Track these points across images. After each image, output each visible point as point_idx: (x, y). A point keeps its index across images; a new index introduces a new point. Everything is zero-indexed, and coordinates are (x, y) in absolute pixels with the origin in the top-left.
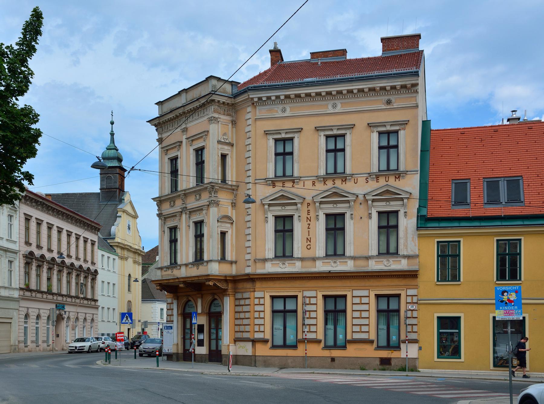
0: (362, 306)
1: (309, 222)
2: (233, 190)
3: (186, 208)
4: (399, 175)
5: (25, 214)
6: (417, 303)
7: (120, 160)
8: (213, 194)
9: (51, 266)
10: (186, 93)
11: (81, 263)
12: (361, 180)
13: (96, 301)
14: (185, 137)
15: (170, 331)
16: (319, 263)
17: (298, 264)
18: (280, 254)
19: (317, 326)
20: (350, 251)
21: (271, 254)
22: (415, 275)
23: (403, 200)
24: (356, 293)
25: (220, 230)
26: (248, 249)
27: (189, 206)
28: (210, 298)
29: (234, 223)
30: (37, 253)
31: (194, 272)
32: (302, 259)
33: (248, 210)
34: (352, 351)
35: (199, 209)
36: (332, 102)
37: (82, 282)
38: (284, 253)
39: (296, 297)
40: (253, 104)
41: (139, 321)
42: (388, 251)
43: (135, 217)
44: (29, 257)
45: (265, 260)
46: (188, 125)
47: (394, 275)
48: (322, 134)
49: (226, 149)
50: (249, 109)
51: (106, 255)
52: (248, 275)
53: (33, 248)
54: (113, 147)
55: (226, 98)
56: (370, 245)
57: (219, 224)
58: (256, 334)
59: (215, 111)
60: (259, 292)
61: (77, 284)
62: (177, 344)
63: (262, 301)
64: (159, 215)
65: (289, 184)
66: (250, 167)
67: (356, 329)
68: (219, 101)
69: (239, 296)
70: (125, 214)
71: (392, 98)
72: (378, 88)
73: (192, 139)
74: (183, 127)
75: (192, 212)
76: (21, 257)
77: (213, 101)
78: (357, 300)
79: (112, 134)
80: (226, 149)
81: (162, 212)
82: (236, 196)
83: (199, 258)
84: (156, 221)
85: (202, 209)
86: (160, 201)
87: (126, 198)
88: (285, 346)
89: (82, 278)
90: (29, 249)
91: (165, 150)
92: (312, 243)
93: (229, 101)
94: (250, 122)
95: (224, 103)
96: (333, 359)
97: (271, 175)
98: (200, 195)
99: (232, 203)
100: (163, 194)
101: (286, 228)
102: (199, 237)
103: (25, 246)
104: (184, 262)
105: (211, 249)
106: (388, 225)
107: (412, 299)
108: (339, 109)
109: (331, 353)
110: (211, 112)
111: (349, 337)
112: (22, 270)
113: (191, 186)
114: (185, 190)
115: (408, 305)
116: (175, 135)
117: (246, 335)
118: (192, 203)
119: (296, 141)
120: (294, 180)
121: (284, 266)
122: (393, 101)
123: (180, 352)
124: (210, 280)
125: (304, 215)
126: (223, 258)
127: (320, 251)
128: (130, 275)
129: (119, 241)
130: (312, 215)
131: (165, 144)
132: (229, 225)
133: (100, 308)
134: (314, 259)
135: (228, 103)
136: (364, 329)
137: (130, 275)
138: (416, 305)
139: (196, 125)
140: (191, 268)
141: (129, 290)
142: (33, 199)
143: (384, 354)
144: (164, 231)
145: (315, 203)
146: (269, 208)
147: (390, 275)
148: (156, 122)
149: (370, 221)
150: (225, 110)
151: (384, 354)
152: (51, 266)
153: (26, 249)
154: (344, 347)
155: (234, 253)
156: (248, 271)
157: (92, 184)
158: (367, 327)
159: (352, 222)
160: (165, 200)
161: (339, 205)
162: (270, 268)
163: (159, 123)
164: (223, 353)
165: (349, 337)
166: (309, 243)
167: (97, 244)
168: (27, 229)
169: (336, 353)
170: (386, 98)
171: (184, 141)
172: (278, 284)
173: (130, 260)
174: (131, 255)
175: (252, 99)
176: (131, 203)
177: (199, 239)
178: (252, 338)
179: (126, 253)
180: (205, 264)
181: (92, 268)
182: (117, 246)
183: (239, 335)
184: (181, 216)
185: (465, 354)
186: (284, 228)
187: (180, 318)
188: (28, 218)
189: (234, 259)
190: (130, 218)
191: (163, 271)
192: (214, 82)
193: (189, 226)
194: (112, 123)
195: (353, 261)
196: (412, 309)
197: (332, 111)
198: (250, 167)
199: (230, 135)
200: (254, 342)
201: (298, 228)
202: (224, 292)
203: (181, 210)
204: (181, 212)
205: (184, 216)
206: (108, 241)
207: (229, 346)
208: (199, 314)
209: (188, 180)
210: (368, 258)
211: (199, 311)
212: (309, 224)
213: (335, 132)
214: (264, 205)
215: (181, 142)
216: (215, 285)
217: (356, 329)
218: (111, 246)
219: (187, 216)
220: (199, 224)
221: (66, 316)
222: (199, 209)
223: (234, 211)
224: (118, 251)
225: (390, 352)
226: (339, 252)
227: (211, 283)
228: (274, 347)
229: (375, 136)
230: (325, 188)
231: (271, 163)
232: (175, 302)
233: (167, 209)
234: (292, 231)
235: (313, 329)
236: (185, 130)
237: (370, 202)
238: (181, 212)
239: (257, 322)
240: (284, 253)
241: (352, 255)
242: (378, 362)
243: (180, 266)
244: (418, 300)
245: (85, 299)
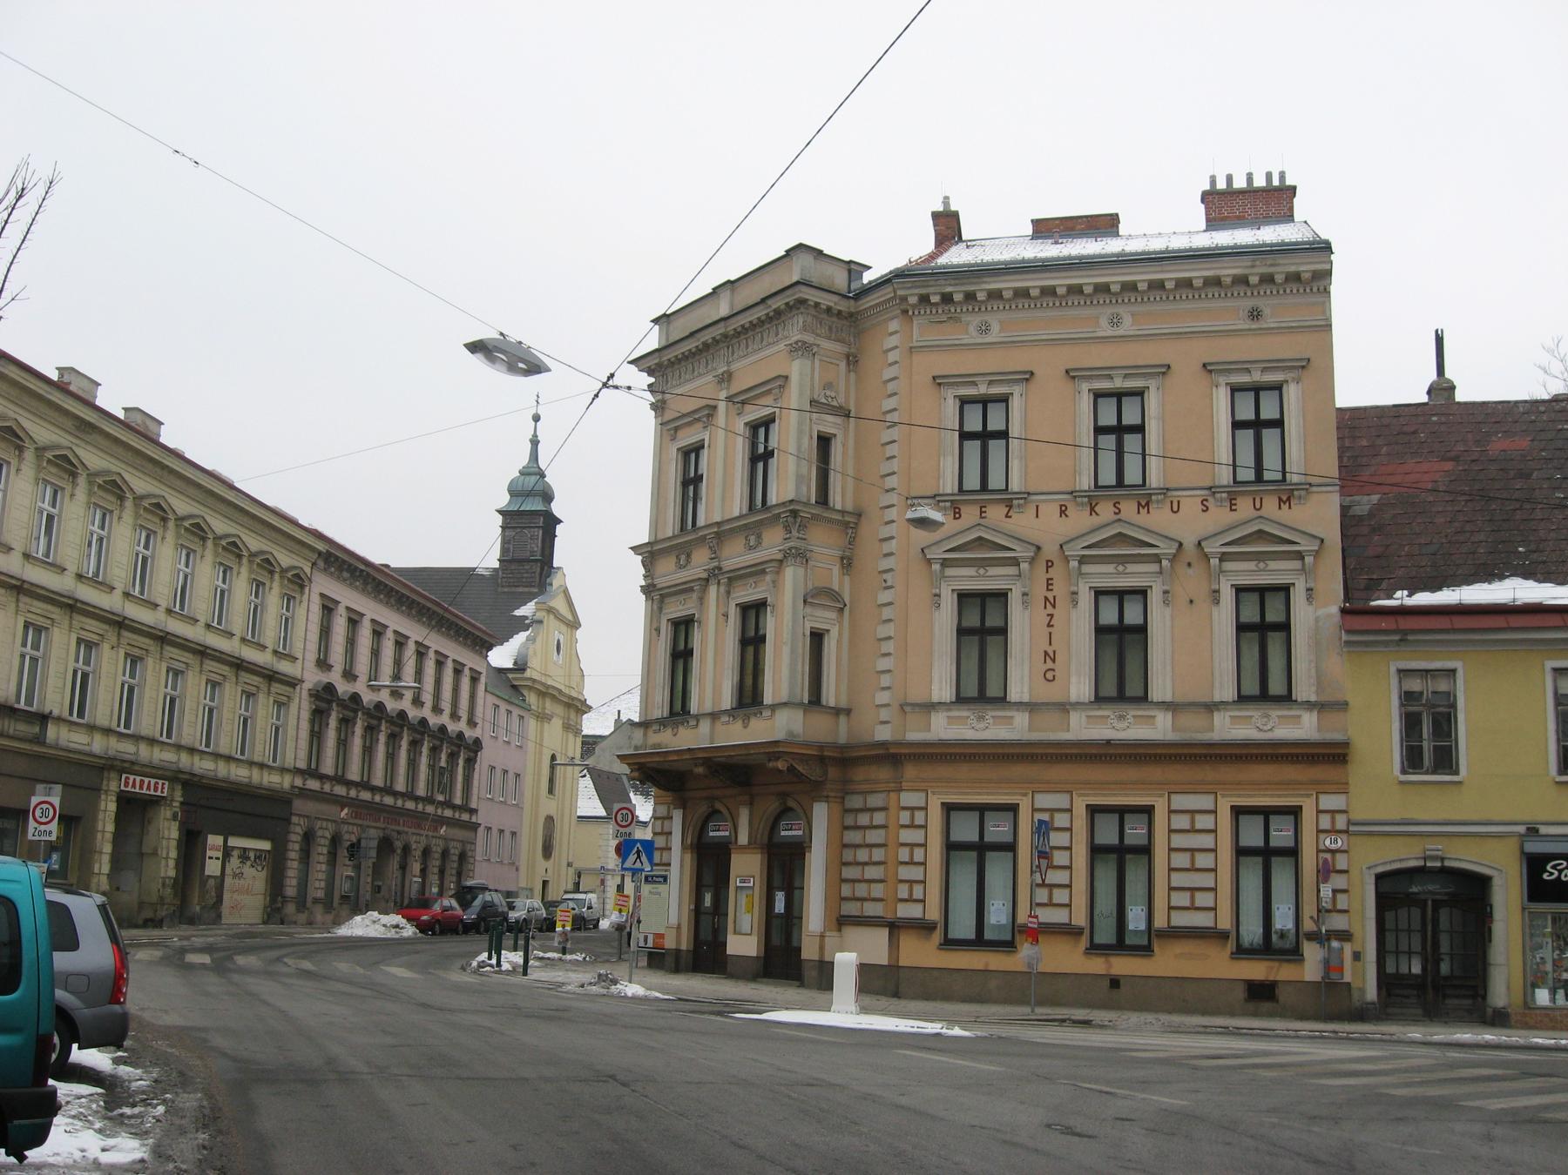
0: (1193, 836)
1: (1050, 609)
2: (846, 525)
3: (720, 568)
4: (1288, 493)
5: (322, 595)
6: (1346, 832)
7: (548, 497)
8: (795, 533)
9: (374, 722)
10: (733, 291)
11: (445, 719)
12: (1191, 505)
13: (473, 811)
14: (723, 395)
15: (662, 888)
16: (1076, 718)
17: (1021, 720)
18: (971, 690)
19: (1072, 891)
20: (1160, 688)
21: (943, 689)
22: (1339, 755)
23: (1303, 558)
24: (1180, 801)
25: (808, 625)
26: (883, 677)
27: (728, 565)
28: (773, 806)
29: (847, 610)
30: (343, 688)
31: (737, 734)
32: (1031, 707)
33: (887, 576)
34: (1167, 962)
35: (756, 572)
36: (1109, 311)
37: (443, 764)
38: (980, 693)
39: (1013, 809)
40: (905, 312)
42: (1263, 692)
43: (574, 624)
44: (324, 697)
45: (930, 707)
46: (734, 367)
47: (1282, 756)
48: (1085, 386)
49: (829, 424)
50: (894, 325)
51: (503, 707)
52: (883, 744)
53: (335, 677)
54: (533, 470)
55: (836, 298)
56: (1217, 674)
57: (808, 610)
58: (900, 906)
59: (805, 329)
60: (910, 794)
61: (431, 767)
62: (679, 927)
63: (919, 818)
64: (647, 590)
65: (996, 513)
66: (894, 465)
67: (1181, 899)
68: (817, 305)
69: (855, 802)
71: (1266, 304)
72: (1229, 280)
73: (740, 401)
74: (720, 371)
75: (736, 578)
76: (305, 694)
77: (802, 302)
78: (1181, 822)
79: (535, 442)
80: (829, 424)
81: (656, 581)
82: (852, 542)
83: (749, 697)
84: (638, 605)
85: (763, 572)
86: (650, 554)
87: (556, 582)
88: (979, 941)
89: (444, 757)
90: (325, 678)
91: (669, 426)
92: (1058, 665)
93: (843, 306)
94: (892, 357)
95: (829, 310)
96: (1115, 983)
97: (949, 485)
98: (759, 537)
99: (842, 558)
100: (660, 536)
101: (989, 623)
102: (752, 642)
103: (315, 670)
104: (708, 707)
105: (782, 673)
106: (1264, 625)
108: (1127, 326)
109: (1110, 966)
110: (795, 330)
111: (1160, 922)
112: (305, 726)
113: (736, 514)
114: (718, 524)
115: (1322, 836)
116: (699, 386)
117: (872, 909)
118: (736, 556)
119: (1016, 404)
120: (1010, 501)
121: (982, 725)
122: (1267, 311)
123: (684, 947)
124: (777, 756)
125: (1040, 591)
126: (815, 700)
127: (1080, 687)
129: (536, 676)
130: (1060, 589)
131: (669, 415)
132: (833, 615)
133: (481, 830)
134: (1064, 707)
135: (840, 312)
136: (1203, 899)
138: (1344, 837)
139: (751, 367)
140: (728, 723)
141: (551, 791)
142: (344, 562)
143: (1257, 970)
144: (658, 630)
145: (1067, 559)
146: (942, 571)
147: (1272, 756)
148: (653, 362)
149: (1215, 610)
150: (830, 329)
151: (1257, 970)
152: (374, 722)
153: (314, 679)
154: (1146, 950)
155: (844, 687)
156: (883, 734)
157: (479, 548)
158: (1211, 895)
159: (1168, 611)
160: (664, 552)
161: (1131, 568)
162: (942, 728)
163: (660, 365)
164: (805, 955)
165: (1160, 922)
166: (1050, 664)
167: (483, 679)
168: (325, 632)
169: (1123, 966)
170: (1249, 303)
171: (722, 406)
172: (964, 771)
173: (557, 723)
175: (904, 299)
176: (566, 593)
177: (751, 649)
178: (890, 916)
179: (550, 706)
180: (767, 713)
181: (469, 734)
182: (530, 688)
183: (851, 909)
184: (704, 589)
186: (982, 622)
187: (688, 857)
188: (328, 607)
189: (843, 704)
190: (564, 628)
191: (650, 732)
192: (805, 260)
193: (726, 615)
194: (536, 418)
195: (1169, 715)
196: (1333, 846)
197: (1109, 333)
198: (894, 465)
199: (842, 387)
200: (895, 927)
201: (1022, 623)
202: (815, 790)
203: (705, 575)
204: (707, 580)
205: (713, 589)
207: (822, 936)
208: (743, 847)
209: (724, 497)
210: (1211, 707)
211: (743, 839)
212: (1052, 616)
213: (1119, 383)
214: (929, 562)
215: (715, 407)
216: (791, 769)
217: (1181, 899)
218: (514, 687)
219: (722, 589)
220: (753, 611)
221: (398, 844)
222: (756, 572)
223: (847, 578)
224: (532, 699)
225: (1276, 964)
226: (1133, 689)
227: (781, 765)
228: (949, 943)
229: (1222, 397)
230: (1096, 520)
231: (949, 459)
232: (678, 816)
233: (669, 572)
234: (1003, 631)
235: (1060, 896)
236: (726, 378)
237: (1214, 562)
238: (707, 580)
239: (905, 873)
240: (980, 693)
241: (1168, 698)
242: (1240, 993)
243: (697, 717)
244: (1349, 823)
245: (448, 804)
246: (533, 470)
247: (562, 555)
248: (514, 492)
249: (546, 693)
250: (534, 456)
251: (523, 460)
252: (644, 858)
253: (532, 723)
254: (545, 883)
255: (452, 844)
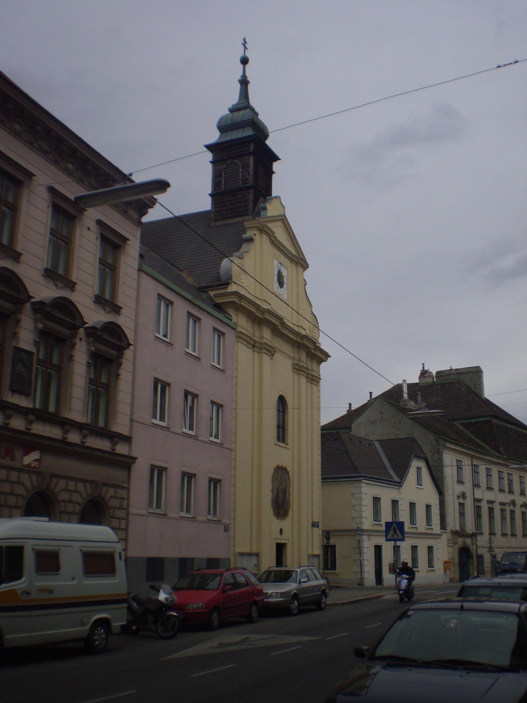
41: (315, 525)
54: (244, 103)
70: (265, 238)
79: (244, 82)
87: (272, 209)
107: (115, 493)
128: (282, 400)
137: (282, 400)
174: (287, 348)
176: (283, 219)
182: (238, 308)
185: (381, 459)
194: (245, 61)
206: (212, 293)
224: (242, 322)
246: (244, 103)
247: (279, 184)
248: (223, 127)
249: (261, 317)
250: (244, 94)
251: (234, 99)
252: (398, 532)
253: (244, 353)
254: (280, 548)
255: (126, 502)
